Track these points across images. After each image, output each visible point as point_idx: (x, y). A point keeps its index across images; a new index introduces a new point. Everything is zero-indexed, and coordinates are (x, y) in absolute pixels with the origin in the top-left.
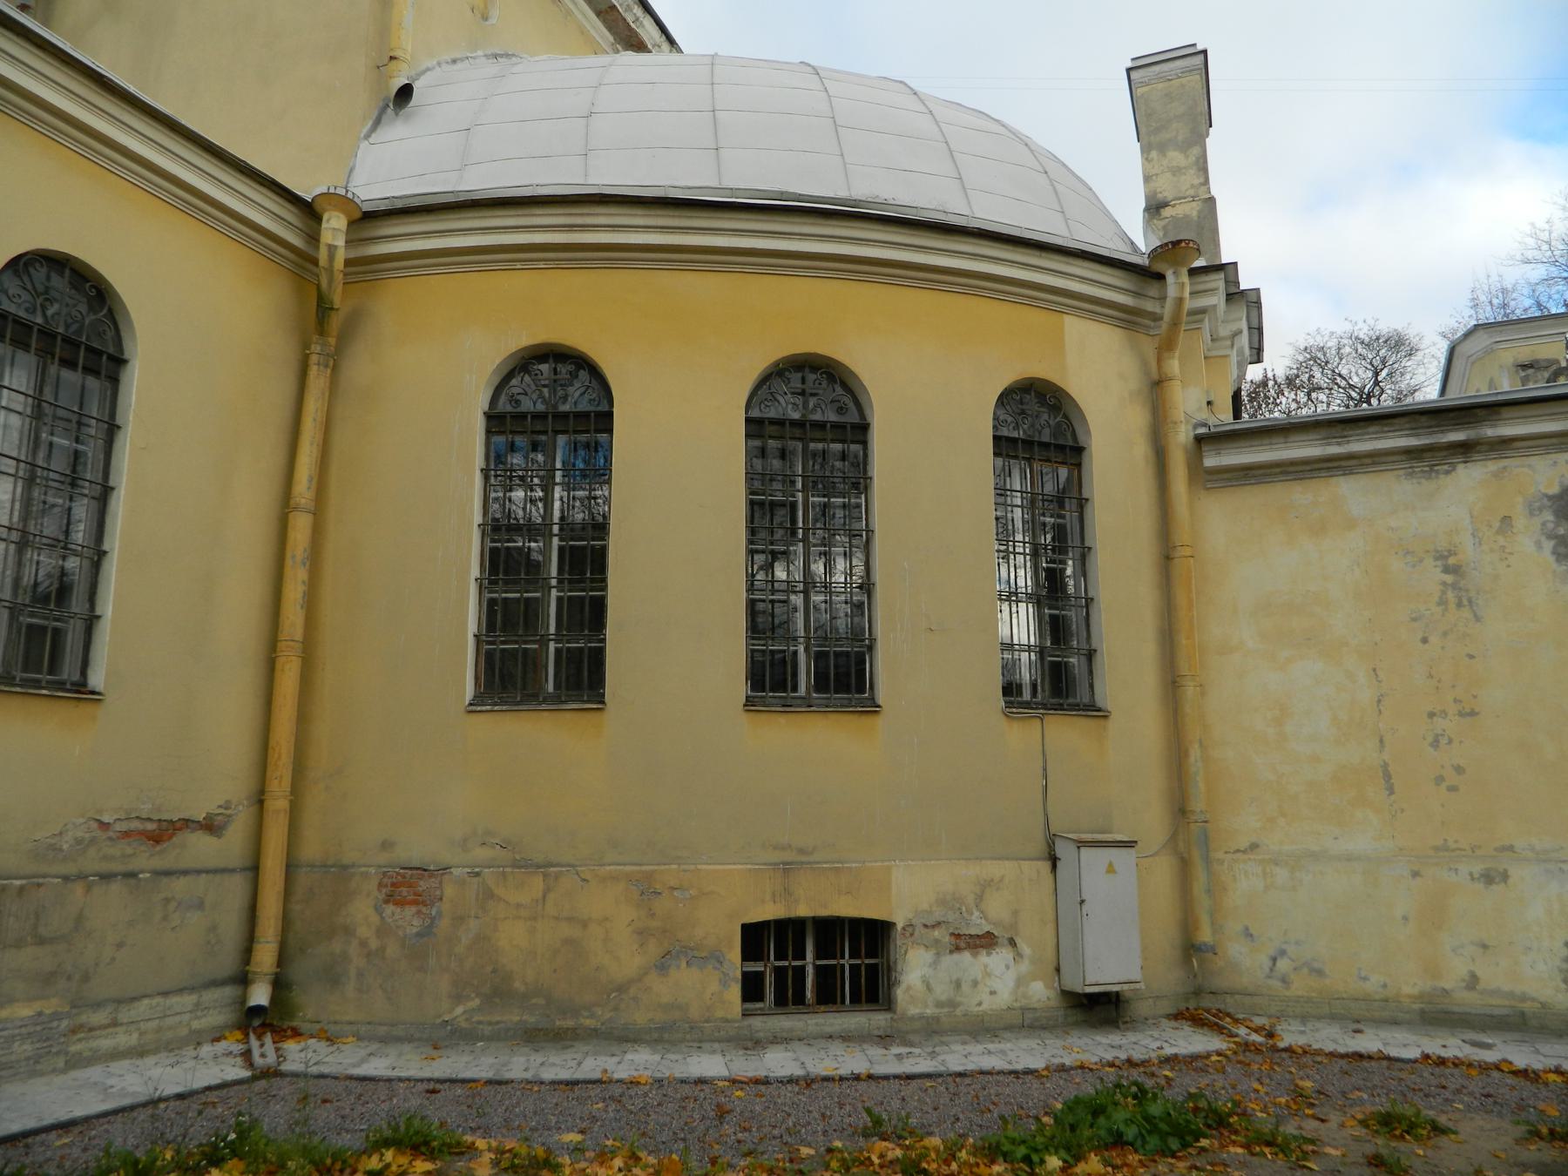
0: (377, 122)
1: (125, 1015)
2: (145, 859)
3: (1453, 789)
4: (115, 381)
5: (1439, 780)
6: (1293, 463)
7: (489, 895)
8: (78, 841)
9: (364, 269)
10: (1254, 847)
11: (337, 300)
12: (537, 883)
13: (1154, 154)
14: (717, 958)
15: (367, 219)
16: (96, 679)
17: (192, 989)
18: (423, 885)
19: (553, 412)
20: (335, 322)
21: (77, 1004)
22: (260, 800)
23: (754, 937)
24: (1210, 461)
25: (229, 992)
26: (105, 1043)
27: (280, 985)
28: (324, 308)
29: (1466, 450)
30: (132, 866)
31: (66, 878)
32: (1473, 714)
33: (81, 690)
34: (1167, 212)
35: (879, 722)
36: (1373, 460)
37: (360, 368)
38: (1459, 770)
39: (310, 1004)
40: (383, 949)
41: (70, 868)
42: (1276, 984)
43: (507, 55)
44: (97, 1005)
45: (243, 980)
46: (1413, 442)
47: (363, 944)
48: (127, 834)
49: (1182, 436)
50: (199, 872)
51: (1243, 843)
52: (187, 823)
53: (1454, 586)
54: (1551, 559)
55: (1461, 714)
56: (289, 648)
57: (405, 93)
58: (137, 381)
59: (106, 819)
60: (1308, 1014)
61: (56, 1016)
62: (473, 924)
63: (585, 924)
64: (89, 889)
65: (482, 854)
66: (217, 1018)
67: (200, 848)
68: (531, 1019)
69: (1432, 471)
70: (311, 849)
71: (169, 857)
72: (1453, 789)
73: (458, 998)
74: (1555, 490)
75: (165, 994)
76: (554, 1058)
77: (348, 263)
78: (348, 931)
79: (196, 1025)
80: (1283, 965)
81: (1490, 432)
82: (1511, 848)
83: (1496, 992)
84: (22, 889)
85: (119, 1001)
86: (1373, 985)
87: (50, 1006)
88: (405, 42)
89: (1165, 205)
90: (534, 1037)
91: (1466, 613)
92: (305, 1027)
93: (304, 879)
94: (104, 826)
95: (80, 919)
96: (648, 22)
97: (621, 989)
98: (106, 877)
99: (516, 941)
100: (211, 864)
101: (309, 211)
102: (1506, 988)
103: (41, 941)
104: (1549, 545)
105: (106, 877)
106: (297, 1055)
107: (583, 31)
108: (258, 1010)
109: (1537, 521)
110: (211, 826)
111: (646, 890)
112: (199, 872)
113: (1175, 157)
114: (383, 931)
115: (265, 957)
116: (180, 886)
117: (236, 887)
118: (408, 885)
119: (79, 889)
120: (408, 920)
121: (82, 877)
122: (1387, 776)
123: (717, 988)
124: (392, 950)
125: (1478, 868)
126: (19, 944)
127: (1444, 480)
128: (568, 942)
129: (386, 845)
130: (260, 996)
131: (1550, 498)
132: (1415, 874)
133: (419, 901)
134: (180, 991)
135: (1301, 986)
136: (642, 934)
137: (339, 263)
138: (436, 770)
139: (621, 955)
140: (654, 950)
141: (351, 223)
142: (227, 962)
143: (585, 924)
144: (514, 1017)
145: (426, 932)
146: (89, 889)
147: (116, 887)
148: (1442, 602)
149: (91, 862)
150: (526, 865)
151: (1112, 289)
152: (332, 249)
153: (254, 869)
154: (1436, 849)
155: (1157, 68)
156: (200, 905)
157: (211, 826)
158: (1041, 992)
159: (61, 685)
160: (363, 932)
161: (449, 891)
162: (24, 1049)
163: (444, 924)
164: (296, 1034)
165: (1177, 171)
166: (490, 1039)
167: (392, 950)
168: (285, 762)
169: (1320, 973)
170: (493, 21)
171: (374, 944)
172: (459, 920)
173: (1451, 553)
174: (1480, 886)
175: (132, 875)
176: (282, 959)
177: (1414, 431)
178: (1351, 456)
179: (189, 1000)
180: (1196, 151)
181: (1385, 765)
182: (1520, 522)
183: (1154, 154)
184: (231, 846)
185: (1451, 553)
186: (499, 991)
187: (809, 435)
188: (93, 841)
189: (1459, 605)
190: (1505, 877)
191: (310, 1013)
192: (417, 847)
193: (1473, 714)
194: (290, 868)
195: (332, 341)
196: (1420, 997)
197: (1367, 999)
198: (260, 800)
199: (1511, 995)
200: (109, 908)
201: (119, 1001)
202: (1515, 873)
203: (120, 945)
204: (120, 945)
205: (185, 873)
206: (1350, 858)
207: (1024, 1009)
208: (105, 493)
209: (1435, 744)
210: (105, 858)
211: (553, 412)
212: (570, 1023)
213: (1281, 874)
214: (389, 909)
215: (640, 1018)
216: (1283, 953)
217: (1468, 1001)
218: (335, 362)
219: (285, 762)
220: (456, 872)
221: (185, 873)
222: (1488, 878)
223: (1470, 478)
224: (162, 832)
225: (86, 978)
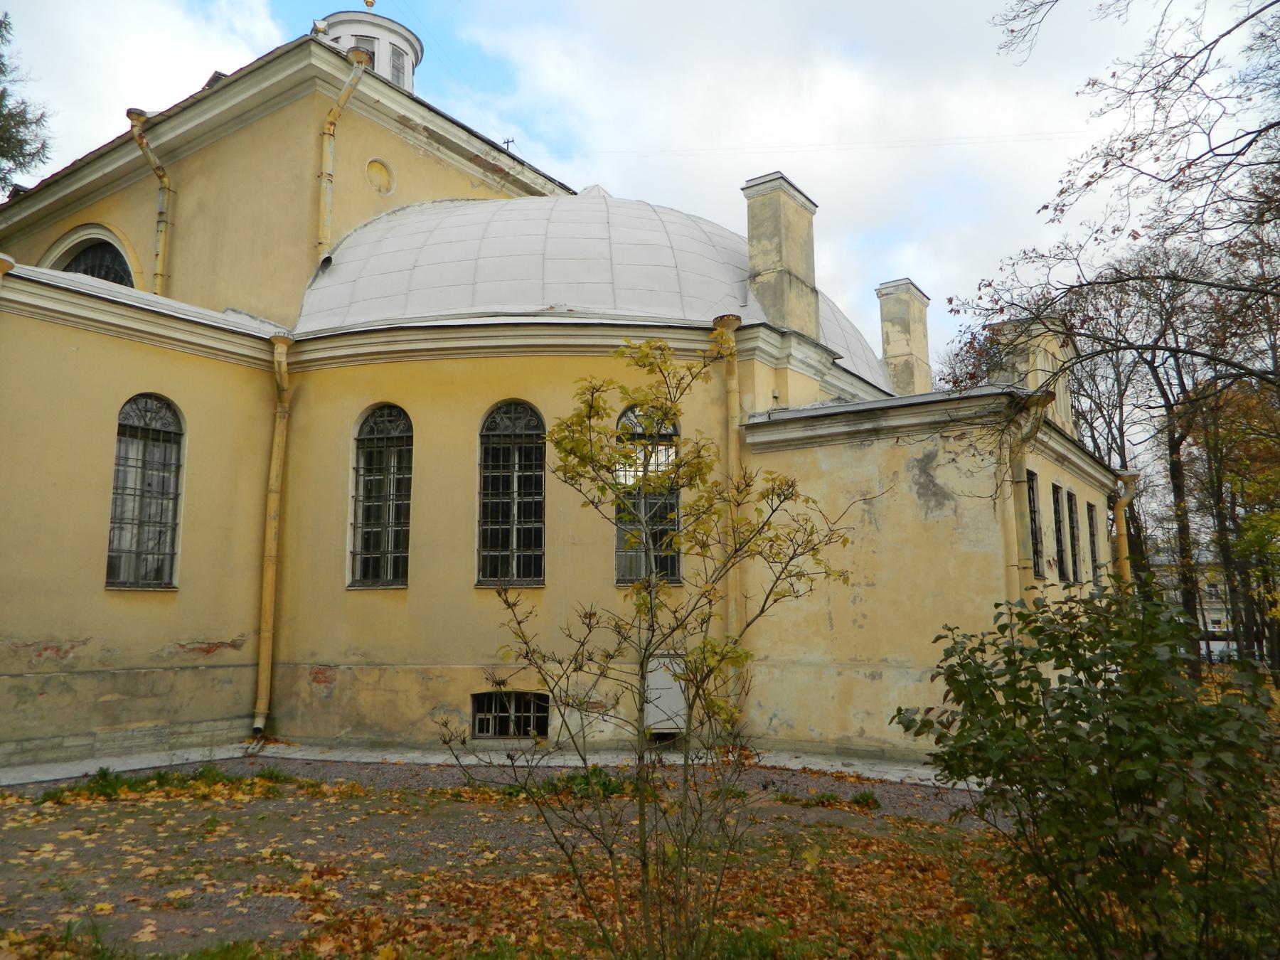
0: (317, 276)
1: (195, 729)
2: (202, 661)
3: (861, 627)
4: (179, 443)
5: (855, 621)
6: (793, 440)
7: (356, 679)
8: (170, 653)
9: (298, 367)
10: (766, 658)
11: (286, 385)
12: (376, 673)
13: (755, 242)
14: (457, 710)
15: (297, 344)
16: (176, 582)
17: (228, 719)
18: (328, 673)
19: (385, 439)
20: (287, 397)
21: (173, 723)
22: (258, 632)
23: (481, 702)
24: (749, 440)
25: (247, 721)
26: (188, 741)
27: (270, 718)
28: (279, 391)
29: (876, 432)
30: (196, 663)
31: (165, 669)
32: (873, 585)
33: (169, 586)
34: (759, 279)
35: (544, 592)
36: (832, 438)
37: (300, 417)
38: (864, 616)
39: (284, 728)
40: (311, 703)
41: (166, 665)
42: (771, 732)
43: (403, 209)
44: (183, 724)
45: (252, 716)
46: (848, 429)
47: (304, 701)
48: (193, 650)
49: (735, 425)
50: (229, 666)
51: (762, 656)
52: (222, 644)
53: (868, 511)
54: (916, 496)
55: (867, 585)
56: (273, 560)
57: (328, 261)
58: (187, 441)
59: (183, 643)
60: (780, 748)
61: (163, 727)
62: (349, 692)
63: (397, 693)
64: (176, 673)
65: (354, 659)
66: (242, 733)
67: (230, 655)
68: (373, 737)
69: (862, 445)
70: (283, 656)
71: (213, 659)
72: (861, 627)
73: (342, 727)
74: (920, 456)
75: (214, 720)
76: (369, 754)
77: (288, 364)
78: (298, 695)
79: (230, 735)
80: (775, 722)
81: (884, 423)
82: (886, 660)
83: (871, 739)
84: (145, 674)
85: (192, 723)
86: (815, 735)
87: (161, 723)
88: (327, 234)
89: (758, 274)
90: (374, 745)
91: (873, 528)
92: (281, 738)
93: (280, 670)
94: (182, 646)
95: (172, 687)
96: (503, 158)
97: (413, 724)
98: (183, 669)
99: (368, 701)
100: (236, 662)
101: (269, 342)
102: (877, 736)
103: (155, 696)
104: (915, 488)
105: (183, 669)
106: (271, 750)
107: (461, 172)
108: (257, 730)
109: (911, 474)
110: (234, 645)
111: (425, 677)
112: (229, 666)
113: (766, 244)
114: (312, 695)
115: (262, 706)
116: (220, 673)
117: (248, 673)
118: (322, 673)
119: (171, 674)
120: (321, 690)
121: (172, 668)
122: (831, 619)
123: (463, 723)
124: (315, 704)
125: (868, 671)
126: (145, 696)
127: (868, 450)
128: (390, 701)
129: (313, 654)
130: (259, 723)
131: (918, 461)
132: (839, 674)
133: (327, 681)
134: (222, 719)
135: (783, 734)
136: (423, 698)
137: (284, 367)
138: (335, 618)
139: (414, 708)
140: (428, 705)
141: (289, 347)
142: (245, 708)
143: (397, 693)
144: (366, 736)
145: (329, 696)
146: (176, 673)
147: (188, 673)
148: (862, 521)
149: (177, 662)
150: (372, 664)
151: (699, 344)
152: (280, 363)
153: (256, 665)
154: (851, 660)
155: (757, 188)
156: (231, 682)
157: (234, 645)
158: (629, 732)
159: (159, 585)
160: (304, 695)
161: (339, 676)
162: (149, 740)
163: (336, 692)
164: (276, 741)
165: (766, 253)
166: (357, 746)
167: (315, 704)
168: (273, 613)
169: (792, 727)
170: (393, 191)
171: (308, 701)
172: (343, 690)
173: (868, 492)
174: (869, 681)
175: (196, 667)
176: (271, 706)
177: (848, 423)
178: (820, 436)
179: (227, 724)
180: (776, 240)
181: (830, 614)
182: (902, 475)
183: (755, 242)
184: (246, 654)
185: (868, 492)
186: (359, 724)
187: (513, 444)
188: (177, 653)
189: (870, 523)
190: (881, 676)
191: (283, 732)
192: (325, 657)
193: (873, 585)
194: (274, 665)
195: (287, 405)
196: (837, 741)
197: (812, 741)
198: (258, 632)
199: (879, 740)
200: (186, 682)
201: (192, 723)
202: (885, 674)
203: (192, 698)
204: (192, 698)
205: (222, 666)
206: (810, 664)
207: (618, 741)
208: (176, 497)
209: (854, 601)
210: (185, 660)
211: (385, 439)
212: (390, 739)
213: (777, 672)
214: (314, 684)
215: (422, 738)
216: (775, 715)
217: (859, 743)
218: (289, 416)
219: (273, 613)
220: (342, 667)
221: (222, 666)
222: (874, 676)
223: (880, 447)
224: (210, 649)
225: (176, 712)
